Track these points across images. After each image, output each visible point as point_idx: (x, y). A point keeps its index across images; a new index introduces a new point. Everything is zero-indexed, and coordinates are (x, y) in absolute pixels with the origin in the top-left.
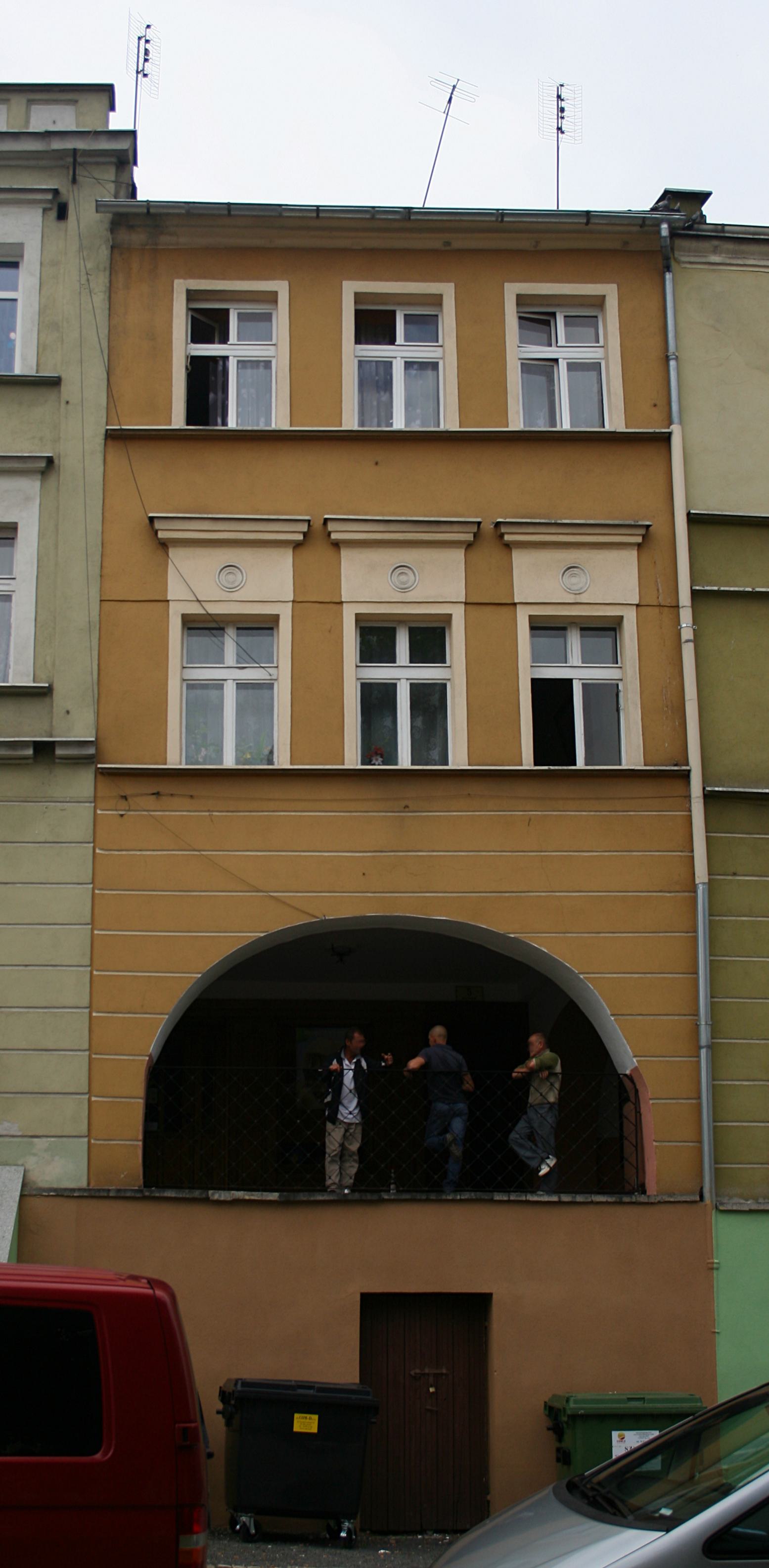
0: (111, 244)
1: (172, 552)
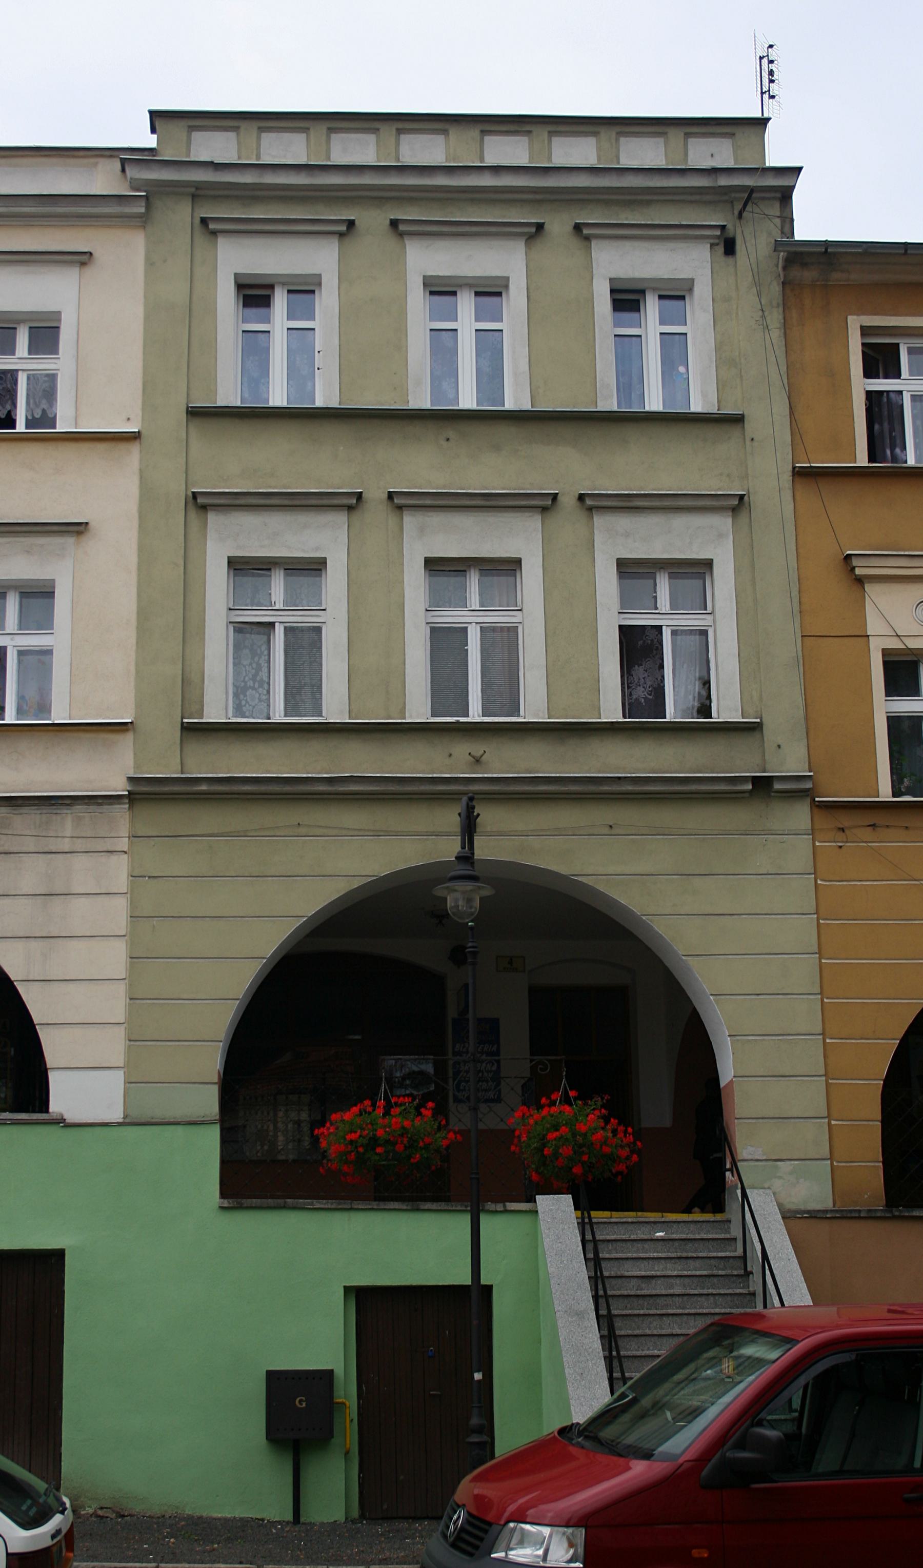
0: (782, 280)
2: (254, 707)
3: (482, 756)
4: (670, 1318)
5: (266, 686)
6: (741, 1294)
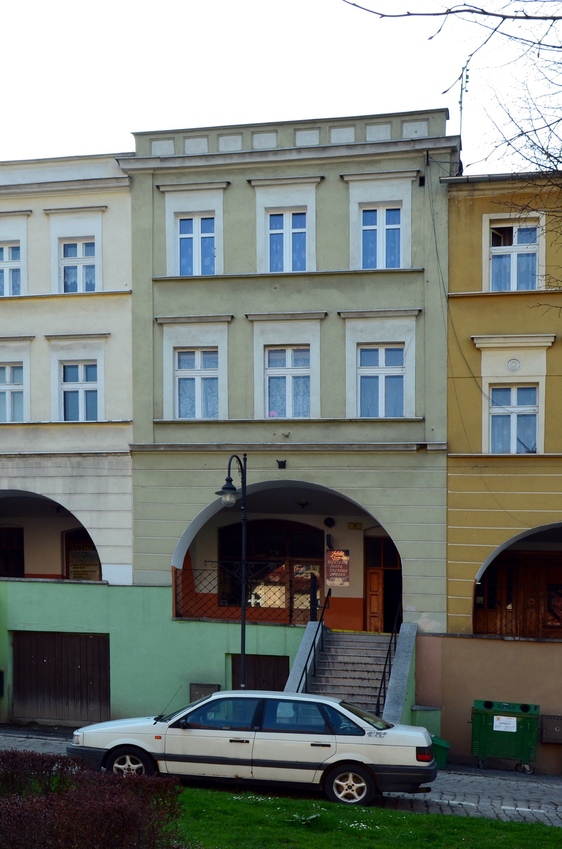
1: (483, 353)
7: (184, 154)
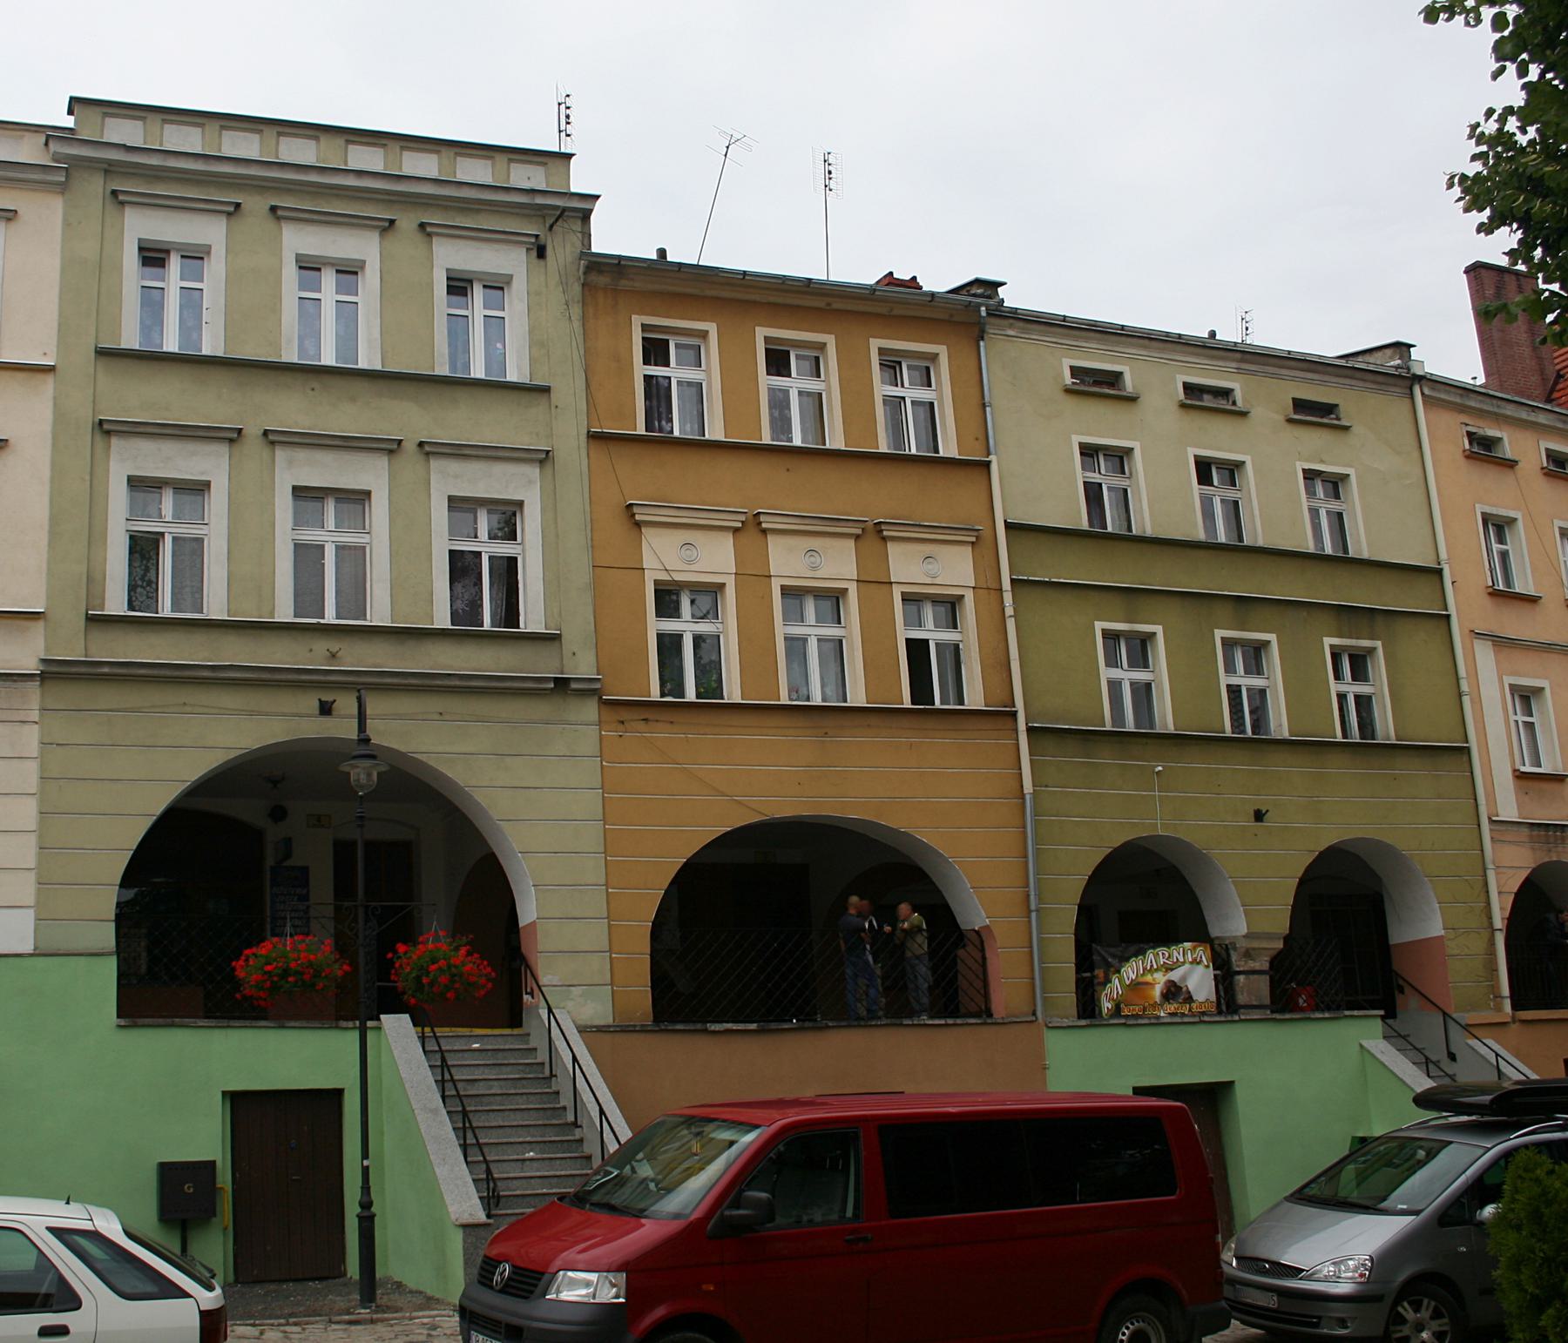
2: (142, 603)
3: (337, 652)
4: (496, 1113)
5: (154, 586)
6: (547, 1093)
7: (161, 145)
